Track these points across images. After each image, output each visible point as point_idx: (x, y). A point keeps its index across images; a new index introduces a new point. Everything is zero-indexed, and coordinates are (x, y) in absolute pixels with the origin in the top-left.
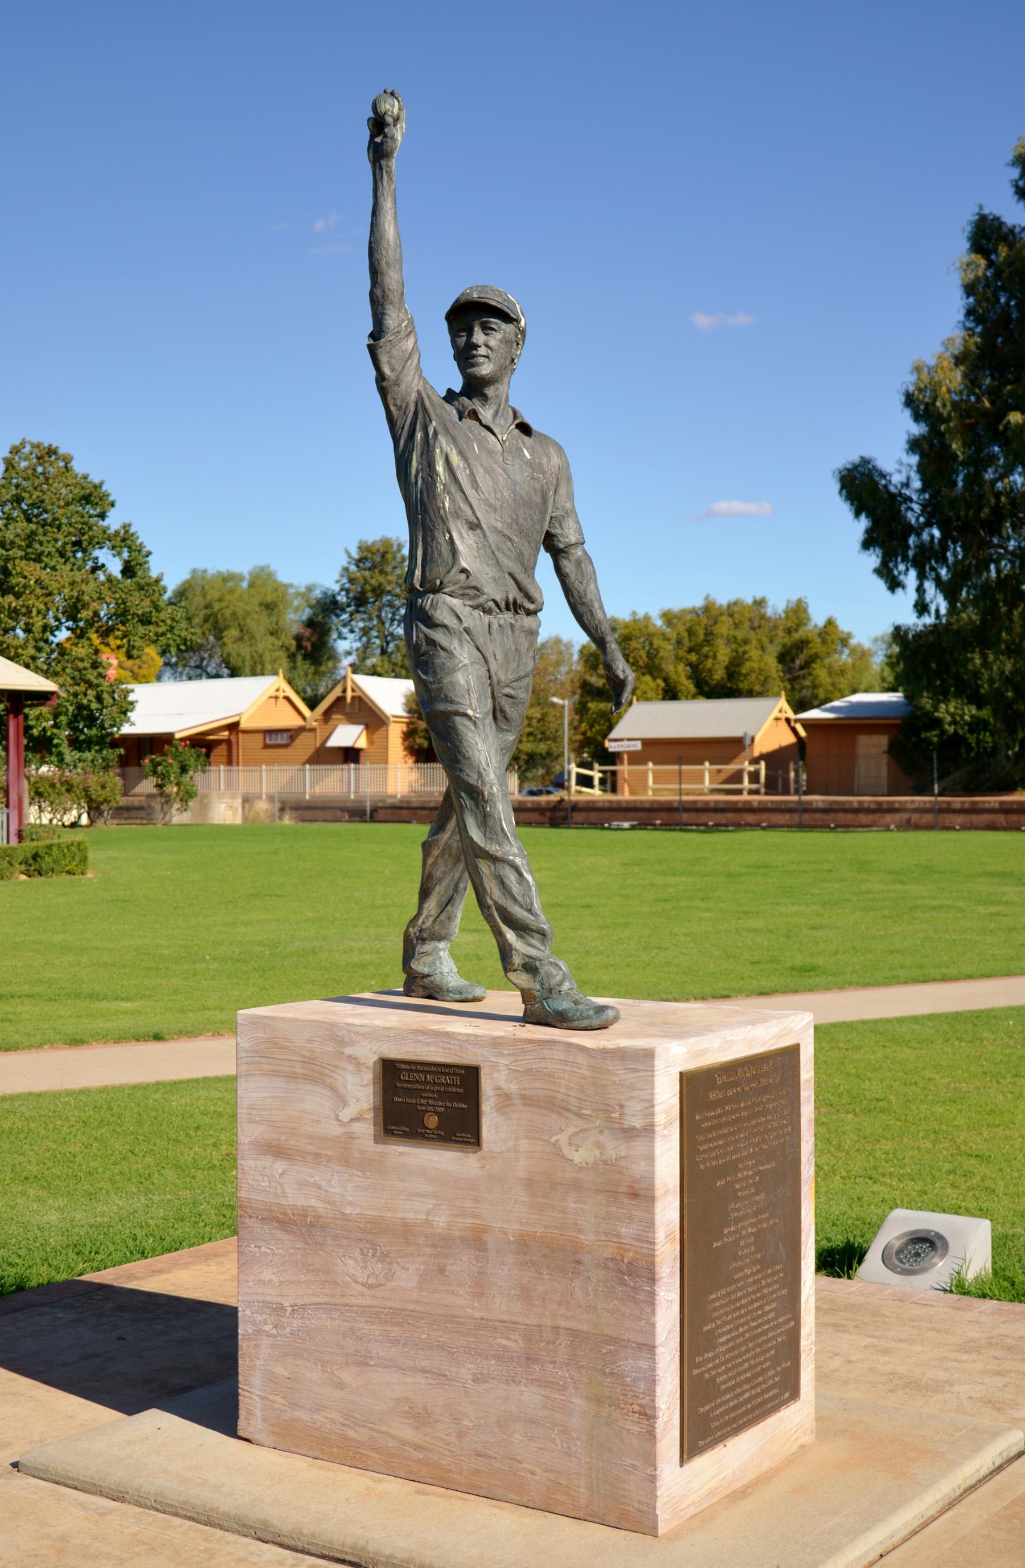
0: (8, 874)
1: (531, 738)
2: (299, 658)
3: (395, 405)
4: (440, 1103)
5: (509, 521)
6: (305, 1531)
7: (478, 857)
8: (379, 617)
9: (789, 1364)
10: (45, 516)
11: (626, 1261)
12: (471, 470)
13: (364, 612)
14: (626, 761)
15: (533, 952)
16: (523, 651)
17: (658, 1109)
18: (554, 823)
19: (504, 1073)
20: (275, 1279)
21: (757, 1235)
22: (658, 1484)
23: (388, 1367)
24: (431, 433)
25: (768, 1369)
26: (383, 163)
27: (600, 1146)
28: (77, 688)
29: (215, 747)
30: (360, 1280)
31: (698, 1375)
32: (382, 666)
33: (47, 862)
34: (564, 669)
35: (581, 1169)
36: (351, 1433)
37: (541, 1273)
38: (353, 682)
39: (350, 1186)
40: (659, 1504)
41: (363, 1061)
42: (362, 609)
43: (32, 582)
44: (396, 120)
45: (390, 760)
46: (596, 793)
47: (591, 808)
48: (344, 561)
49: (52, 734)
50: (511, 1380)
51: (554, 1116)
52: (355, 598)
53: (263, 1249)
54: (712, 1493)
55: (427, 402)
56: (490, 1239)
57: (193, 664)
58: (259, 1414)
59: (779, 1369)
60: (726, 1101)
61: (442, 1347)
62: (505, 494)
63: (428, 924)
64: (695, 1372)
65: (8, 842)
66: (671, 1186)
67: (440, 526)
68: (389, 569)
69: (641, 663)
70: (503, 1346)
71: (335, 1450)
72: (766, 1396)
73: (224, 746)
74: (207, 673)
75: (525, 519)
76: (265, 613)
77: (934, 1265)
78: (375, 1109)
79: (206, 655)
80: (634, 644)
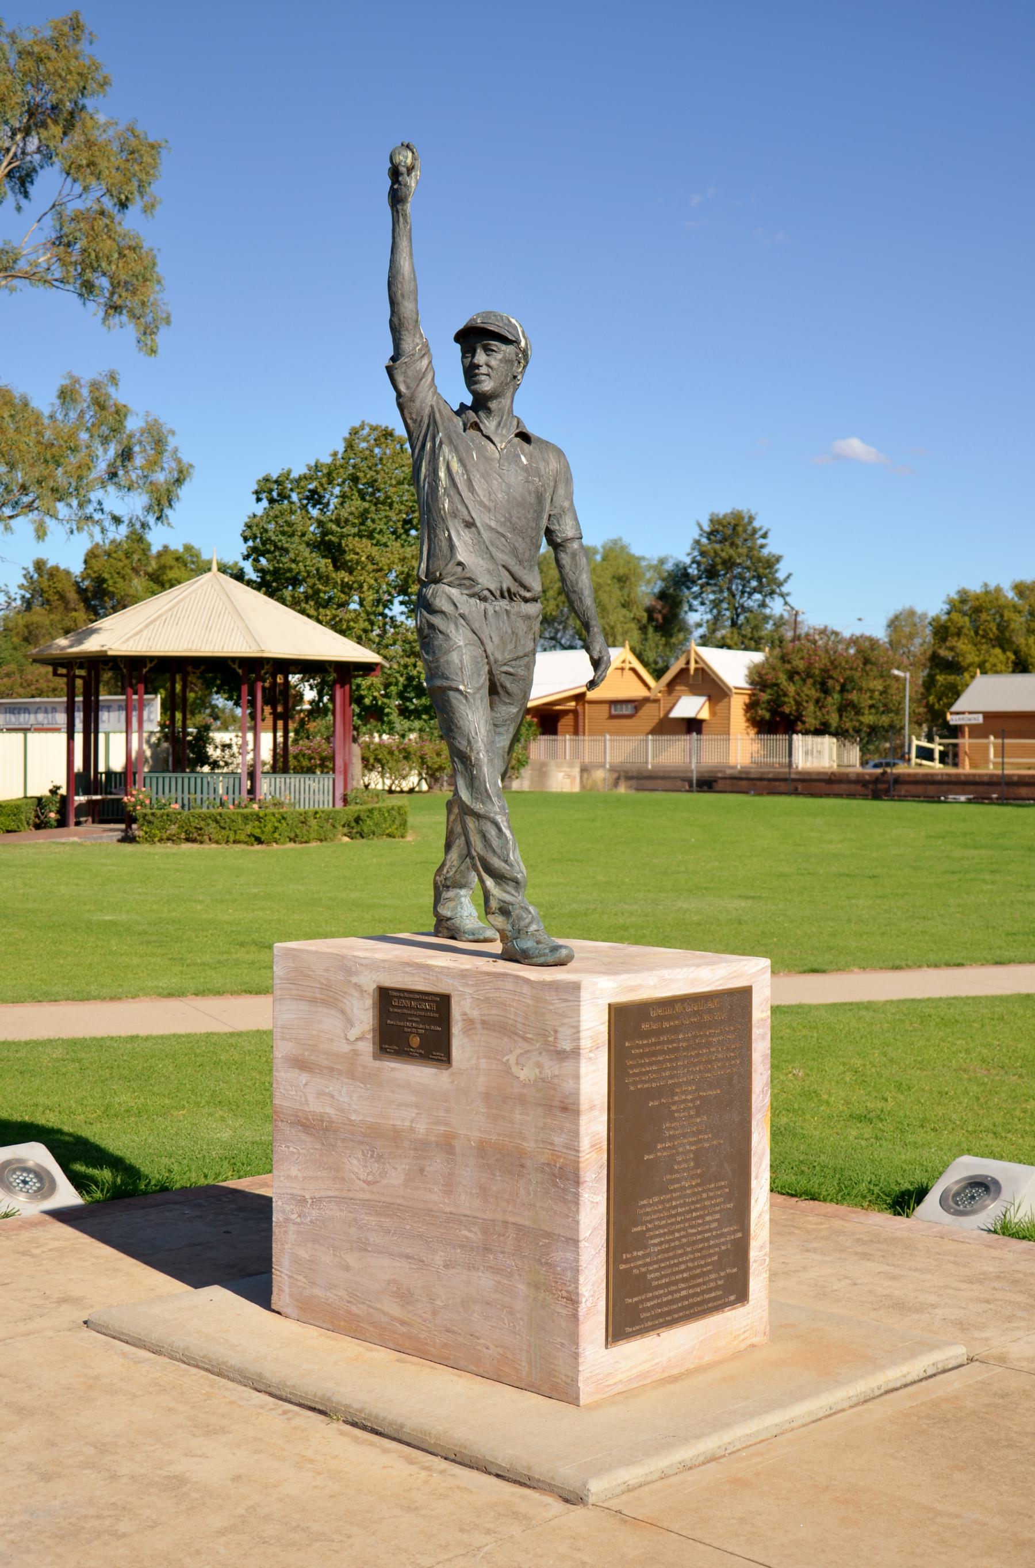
0: (331, 836)
1: (873, 711)
2: (651, 630)
3: (411, 418)
4: (421, 1026)
5: (503, 519)
6: (288, 1384)
7: (466, 814)
8: (729, 589)
9: (735, 1270)
10: (378, 495)
11: (558, 1166)
12: (468, 475)
13: (715, 585)
14: (967, 734)
15: (508, 898)
16: (521, 633)
17: (583, 1034)
18: (876, 796)
19: (469, 1000)
20: (299, 1175)
21: (698, 1154)
22: (581, 1360)
23: (381, 1253)
24: (437, 443)
25: (709, 1272)
26: (399, 207)
27: (539, 1065)
28: (407, 660)
29: (562, 717)
30: (362, 1177)
31: (625, 1270)
32: (732, 639)
33: (368, 825)
34: (918, 641)
35: (525, 1086)
36: (354, 1309)
37: (494, 1175)
38: (696, 653)
39: (355, 1096)
40: (580, 1378)
41: (365, 988)
42: (712, 582)
43: (363, 559)
44: (410, 170)
45: (732, 731)
46: (936, 766)
47: (929, 781)
48: (696, 534)
49: (383, 703)
50: (472, 1267)
51: (506, 1039)
52: (706, 570)
53: (291, 1149)
54: (642, 1375)
55: (437, 415)
56: (457, 1144)
57: (547, 636)
58: (287, 1290)
59: (722, 1274)
60: (661, 1032)
61: (420, 1236)
62: (500, 496)
63: (451, 873)
64: (622, 1267)
65: (334, 805)
66: (597, 1102)
67: (441, 525)
68: (739, 542)
69: (991, 635)
70: (466, 1237)
71: (342, 1323)
72: (707, 1296)
73: (571, 716)
74: (561, 644)
75: (519, 518)
76: (617, 585)
77: (985, 1207)
78: (374, 1030)
79: (561, 627)
80: (984, 616)
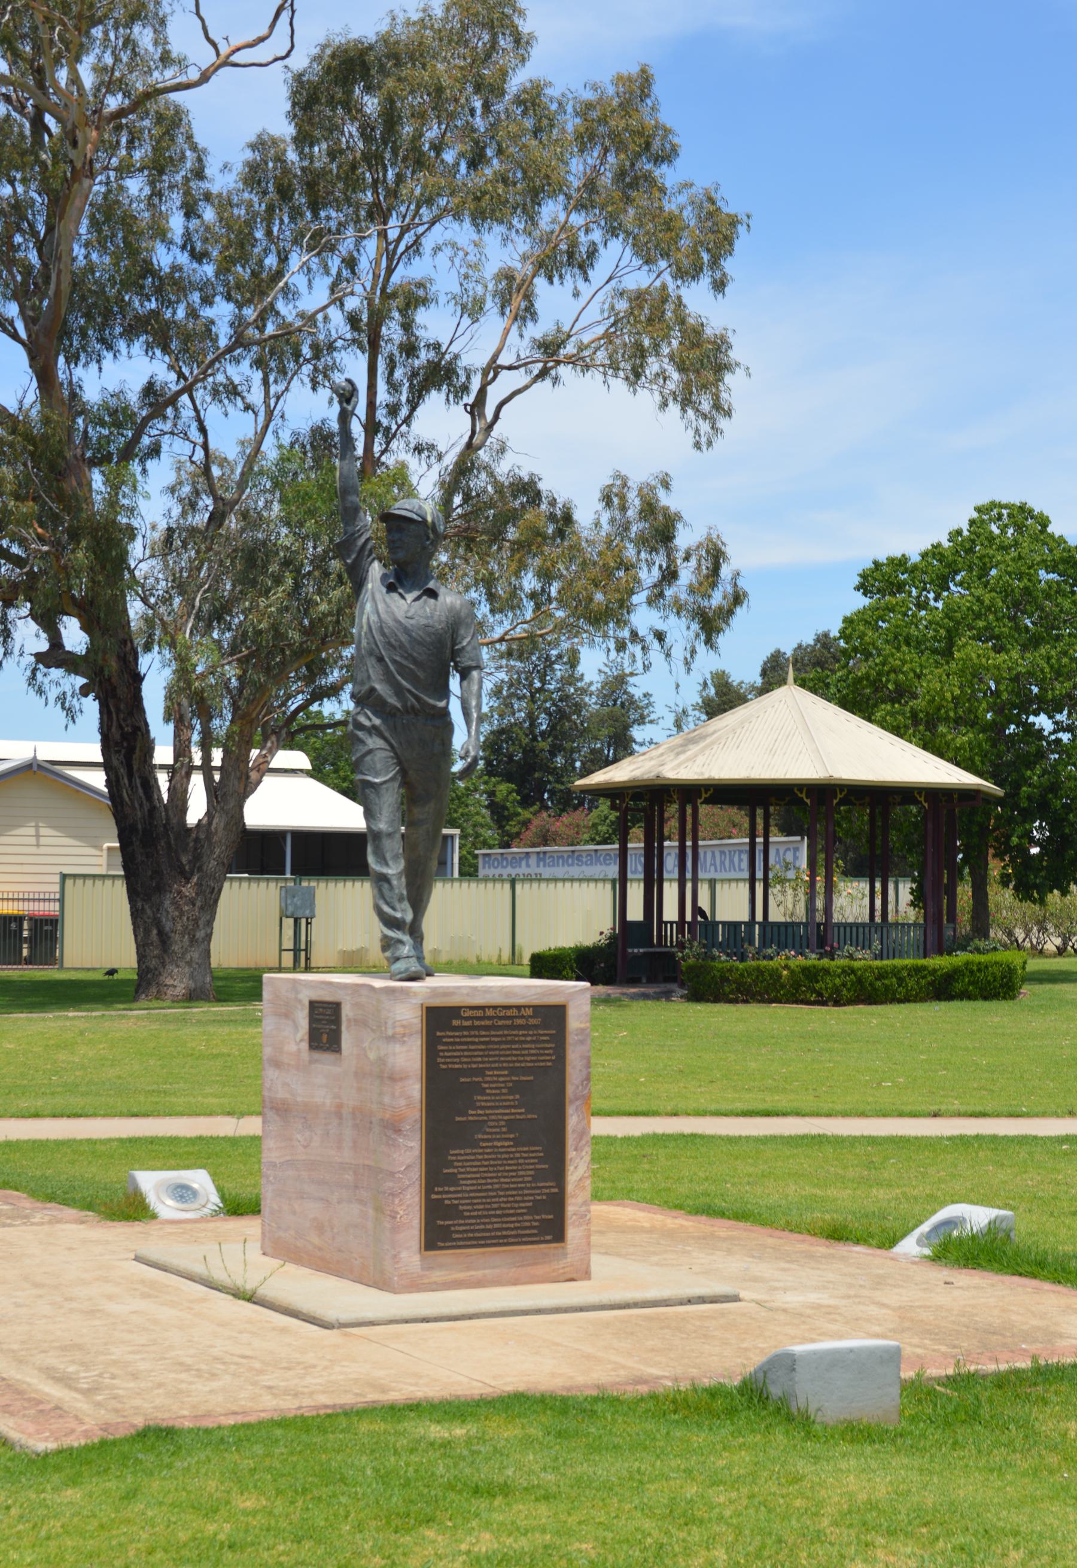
64: (434, 1197)
